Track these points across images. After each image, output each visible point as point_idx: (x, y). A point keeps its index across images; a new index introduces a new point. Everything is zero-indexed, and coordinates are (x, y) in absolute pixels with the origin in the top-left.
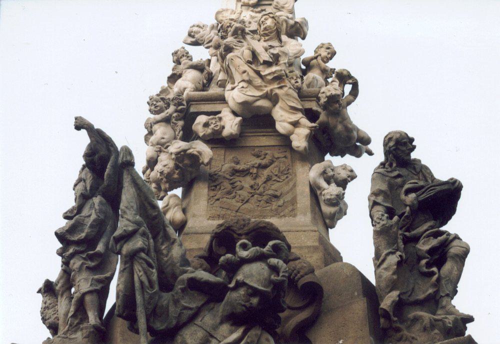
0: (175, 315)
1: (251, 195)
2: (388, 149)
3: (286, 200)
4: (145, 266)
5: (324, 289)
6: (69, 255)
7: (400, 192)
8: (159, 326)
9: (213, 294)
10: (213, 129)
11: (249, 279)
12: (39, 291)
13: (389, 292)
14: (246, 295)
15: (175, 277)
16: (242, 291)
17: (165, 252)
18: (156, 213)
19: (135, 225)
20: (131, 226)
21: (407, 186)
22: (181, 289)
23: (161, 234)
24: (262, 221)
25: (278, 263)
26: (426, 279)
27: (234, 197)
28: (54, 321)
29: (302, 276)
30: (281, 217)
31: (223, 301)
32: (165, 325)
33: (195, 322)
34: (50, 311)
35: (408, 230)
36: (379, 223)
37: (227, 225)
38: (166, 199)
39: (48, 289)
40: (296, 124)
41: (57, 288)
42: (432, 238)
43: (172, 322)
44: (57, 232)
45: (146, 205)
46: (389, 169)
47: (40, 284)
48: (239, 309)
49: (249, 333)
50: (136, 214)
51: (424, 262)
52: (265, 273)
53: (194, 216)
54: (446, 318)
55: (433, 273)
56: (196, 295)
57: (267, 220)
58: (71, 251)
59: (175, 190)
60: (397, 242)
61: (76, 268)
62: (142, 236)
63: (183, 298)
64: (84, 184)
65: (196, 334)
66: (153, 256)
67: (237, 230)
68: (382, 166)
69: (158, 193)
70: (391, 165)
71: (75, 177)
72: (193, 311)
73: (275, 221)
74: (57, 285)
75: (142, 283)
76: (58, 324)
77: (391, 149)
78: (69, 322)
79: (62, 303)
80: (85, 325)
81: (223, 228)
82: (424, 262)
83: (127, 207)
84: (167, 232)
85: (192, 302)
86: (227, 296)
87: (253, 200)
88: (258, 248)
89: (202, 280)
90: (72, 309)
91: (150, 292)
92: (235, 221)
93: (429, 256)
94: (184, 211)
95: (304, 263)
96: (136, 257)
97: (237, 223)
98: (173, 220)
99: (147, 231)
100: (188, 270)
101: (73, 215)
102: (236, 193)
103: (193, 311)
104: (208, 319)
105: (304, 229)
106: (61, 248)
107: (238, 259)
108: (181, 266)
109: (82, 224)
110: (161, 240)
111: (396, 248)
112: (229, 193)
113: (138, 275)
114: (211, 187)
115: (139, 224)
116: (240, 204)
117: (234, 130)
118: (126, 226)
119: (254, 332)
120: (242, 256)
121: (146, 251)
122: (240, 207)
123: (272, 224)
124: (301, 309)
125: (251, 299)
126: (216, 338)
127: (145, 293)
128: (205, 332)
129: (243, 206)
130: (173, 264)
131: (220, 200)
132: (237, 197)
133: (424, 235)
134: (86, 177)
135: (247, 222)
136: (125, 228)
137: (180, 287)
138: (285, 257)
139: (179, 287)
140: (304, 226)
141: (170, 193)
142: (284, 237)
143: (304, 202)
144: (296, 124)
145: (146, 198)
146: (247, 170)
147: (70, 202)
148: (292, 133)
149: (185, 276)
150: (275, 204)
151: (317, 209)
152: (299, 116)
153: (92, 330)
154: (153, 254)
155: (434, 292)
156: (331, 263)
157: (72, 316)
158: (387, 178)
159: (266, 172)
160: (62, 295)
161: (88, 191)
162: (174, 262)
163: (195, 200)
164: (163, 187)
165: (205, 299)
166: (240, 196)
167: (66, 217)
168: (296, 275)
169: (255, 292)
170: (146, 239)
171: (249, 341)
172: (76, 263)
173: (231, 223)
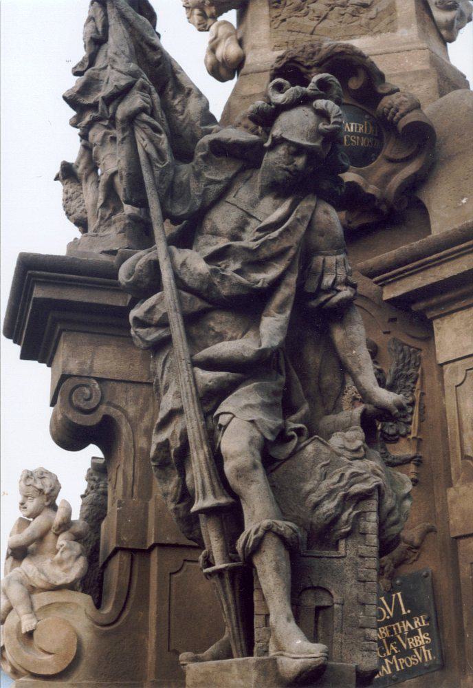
0: (198, 194)
1: (329, 8)
3: (380, 9)
4: (149, 131)
5: (436, 130)
6: (87, 124)
8: (180, 210)
9: (245, 157)
11: (289, 132)
12: (57, 178)
14: (287, 155)
15: (195, 139)
16: (281, 151)
17: (179, 108)
18: (159, 56)
19: (129, 77)
20: (125, 79)
22: (201, 156)
23: (170, 84)
24: (338, 44)
25: (326, 105)
27: (306, 14)
28: (81, 215)
29: (403, 115)
30: (375, 34)
31: (260, 167)
32: (188, 208)
33: (227, 200)
34: (74, 203)
37: (290, 56)
38: (213, 28)
39: (67, 173)
41: (79, 171)
43: (195, 202)
44: (65, 95)
47: (57, 169)
48: (280, 176)
49: (298, 207)
50: (129, 62)
52: (310, 122)
53: (253, 47)
56: (224, 162)
57: (345, 42)
58: (87, 118)
59: (225, 14)
61: (97, 142)
62: (141, 91)
63: (206, 168)
64: (93, 24)
65: (230, 215)
66: (160, 116)
67: (304, 61)
69: (204, 21)
71: (86, 16)
72: (222, 185)
73: (361, 44)
74: (78, 167)
75: (148, 155)
76: (87, 218)
78: (100, 214)
79: (89, 189)
80: (118, 215)
81: (284, 61)
83: (116, 54)
84: (178, 80)
85: (219, 174)
86: (264, 159)
87: (333, 15)
88: (297, 87)
89: (230, 141)
90: (101, 197)
91: (161, 166)
92: (301, 49)
94: (241, 42)
95: (405, 96)
96: (136, 121)
97: (303, 51)
98: (226, 56)
99: (148, 82)
100: (212, 130)
101: (84, 69)
102: (308, 7)
103: (222, 185)
104: (243, 194)
105: (408, 47)
106: (74, 117)
108: (202, 124)
109: (97, 80)
110: (171, 93)
112: (299, 9)
113: (142, 145)
114: (273, 3)
115: (134, 75)
116: (316, 22)
118: (118, 81)
119: (306, 205)
120: (276, 101)
121: (149, 111)
122: (315, 27)
123: (352, 47)
124: (407, 160)
125: (295, 159)
126: (255, 218)
127: (154, 169)
128: (240, 212)
129: (319, 25)
130: (192, 124)
131: (287, 20)
132: (311, 13)
134: (95, 13)
135: (318, 48)
136: (115, 83)
137: (200, 154)
138: (337, 96)
139: (199, 154)
140: (408, 43)
141: (220, 19)
142: (373, 62)
143: (405, 8)
145: (143, 38)
147: (79, 53)
149: (206, 139)
150: (365, 16)
151: (426, 16)
153: (127, 221)
154: (159, 113)
156: (450, 91)
157: (102, 206)
160: (86, 179)
161: (101, 33)
162: (192, 121)
163: (253, 25)
164: (208, 12)
165: (239, 166)
166: (314, 11)
167: (77, 74)
168: (394, 115)
169: (299, 150)
171: (298, 216)
172: (96, 134)
173: (295, 53)
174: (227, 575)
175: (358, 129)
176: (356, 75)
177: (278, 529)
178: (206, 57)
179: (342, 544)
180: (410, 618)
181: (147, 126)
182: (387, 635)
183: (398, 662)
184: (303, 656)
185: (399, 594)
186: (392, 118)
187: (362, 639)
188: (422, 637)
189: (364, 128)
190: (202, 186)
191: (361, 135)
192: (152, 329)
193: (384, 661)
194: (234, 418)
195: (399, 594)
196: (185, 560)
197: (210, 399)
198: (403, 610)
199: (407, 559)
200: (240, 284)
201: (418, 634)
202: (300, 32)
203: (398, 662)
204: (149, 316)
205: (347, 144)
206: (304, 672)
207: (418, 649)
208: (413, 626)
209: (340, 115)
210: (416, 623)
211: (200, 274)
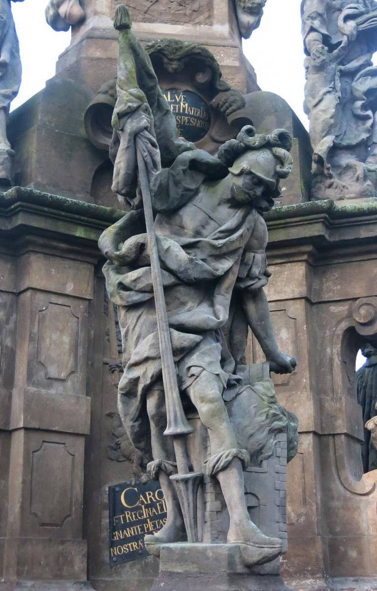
7: (338, 16)
13: (325, 136)
21: (346, 12)
22: (183, 170)
26: (360, 123)
29: (234, 111)
30: (196, 24)
35: (342, 63)
42: (370, 77)
45: (143, 72)
51: (359, 103)
53: (96, 13)
55: (367, 118)
60: (334, 80)
75: (146, 163)
82: (359, 103)
89: (203, 161)
93: (365, 98)
96: (140, 136)
107: (244, 146)
111: (333, 86)
122: (149, 8)
129: (153, 7)
133: (363, 72)
143: (221, 7)
149: (188, 155)
155: (367, 138)
168: (227, 108)
170: (148, 116)
174: (190, 483)
175: (196, 113)
176: (203, 72)
177: (242, 456)
178: (48, 8)
179: (265, 463)
181: (148, 142)
184: (266, 546)
186: (225, 111)
187: (278, 530)
189: (200, 113)
190: (180, 191)
191: (198, 118)
194: (204, 371)
196: (44, 441)
197: (181, 354)
200: (206, 271)
202: (135, 9)
204: (133, 284)
205: (187, 123)
206: (265, 557)
209: (292, 163)
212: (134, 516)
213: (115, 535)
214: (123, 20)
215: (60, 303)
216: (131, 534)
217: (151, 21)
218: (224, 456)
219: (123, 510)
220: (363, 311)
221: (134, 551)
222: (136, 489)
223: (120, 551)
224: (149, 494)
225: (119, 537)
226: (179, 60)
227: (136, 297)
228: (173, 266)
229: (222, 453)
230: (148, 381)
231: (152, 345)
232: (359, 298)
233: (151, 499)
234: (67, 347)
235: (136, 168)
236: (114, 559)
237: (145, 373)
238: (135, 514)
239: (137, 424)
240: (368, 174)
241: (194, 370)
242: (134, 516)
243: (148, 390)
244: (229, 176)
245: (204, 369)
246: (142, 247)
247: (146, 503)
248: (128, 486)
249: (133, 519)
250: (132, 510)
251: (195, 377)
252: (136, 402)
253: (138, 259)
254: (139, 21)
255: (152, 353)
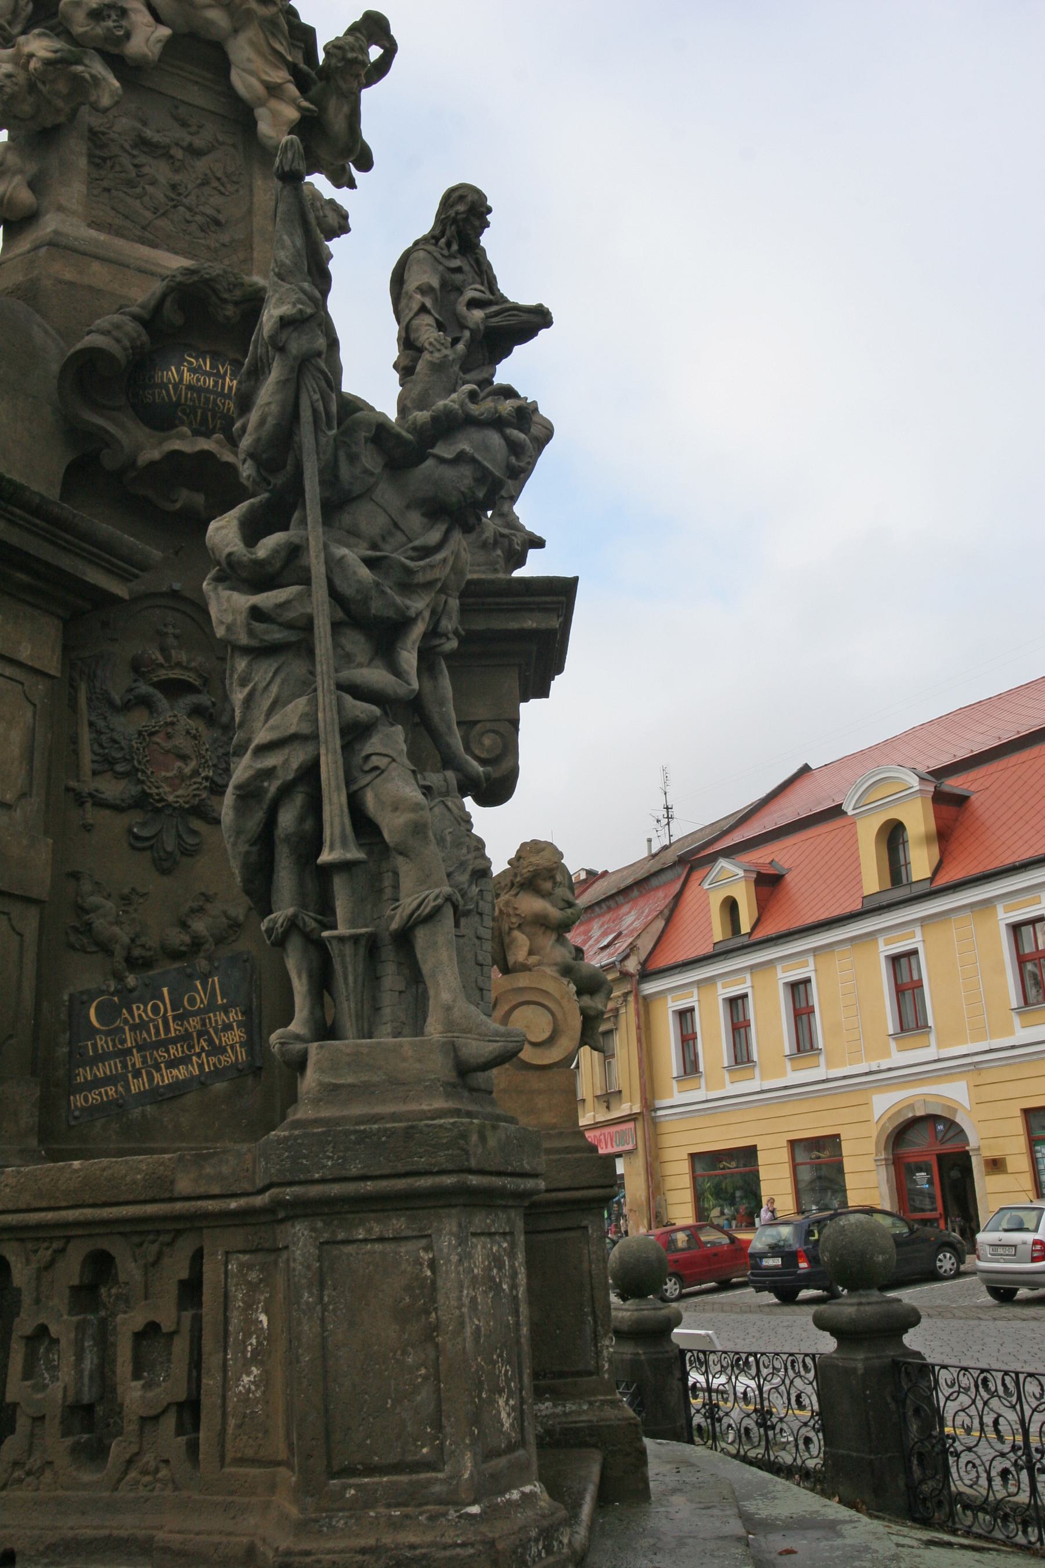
1: (171, 204)
2: (453, 215)
10: (108, 29)
36: (439, 350)
40: (273, 90)
46: (446, 252)
54: (515, 535)
68: (433, 241)
70: (449, 245)
77: (459, 217)
81: (196, 278)
113: (310, 397)
117: (153, 54)
126: (402, 531)
144: (273, 90)
146: (164, 147)
148: (263, 104)
152: (280, 76)
158: (441, 268)
159: (201, 165)
174: (363, 942)
180: (225, 1009)
182: (199, 1027)
183: (208, 1062)
185: (216, 979)
188: (237, 1032)
192: (275, 627)
193: (191, 1060)
195: (216, 979)
197: (354, 734)
198: (219, 998)
199: (225, 938)
201: (233, 1029)
203: (208, 1062)
207: (232, 1047)
208: (228, 1018)
210: (232, 1015)
211: (359, 581)
212: (110, 1044)
213: (79, 1074)
214: (295, 164)
215: (7, 674)
216: (105, 1073)
217: (154, 245)
218: (432, 897)
219: (93, 1032)
220: (487, 741)
221: (110, 1102)
222: (116, 999)
223: (86, 1100)
224: (138, 1008)
225: (85, 1078)
226: (236, 304)
227: (277, 635)
228: (347, 590)
229: (427, 892)
230: (291, 776)
231: (304, 717)
232: (479, 721)
233: (140, 1016)
234: (17, 752)
235: (295, 416)
236: (77, 1113)
237: (286, 762)
238: (113, 1040)
239: (254, 849)
240: (500, 539)
241: (375, 761)
242: (110, 1044)
243: (286, 791)
244: (429, 463)
245: (394, 760)
246: (295, 551)
247: (131, 1022)
248: (102, 992)
249: (108, 1047)
250: (108, 1033)
251: (378, 772)
252: (258, 816)
253: (289, 567)
254: (133, 240)
255: (305, 729)
